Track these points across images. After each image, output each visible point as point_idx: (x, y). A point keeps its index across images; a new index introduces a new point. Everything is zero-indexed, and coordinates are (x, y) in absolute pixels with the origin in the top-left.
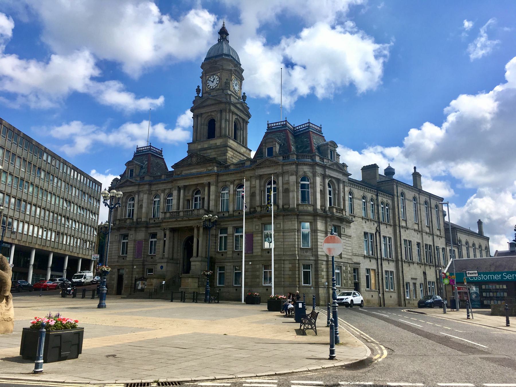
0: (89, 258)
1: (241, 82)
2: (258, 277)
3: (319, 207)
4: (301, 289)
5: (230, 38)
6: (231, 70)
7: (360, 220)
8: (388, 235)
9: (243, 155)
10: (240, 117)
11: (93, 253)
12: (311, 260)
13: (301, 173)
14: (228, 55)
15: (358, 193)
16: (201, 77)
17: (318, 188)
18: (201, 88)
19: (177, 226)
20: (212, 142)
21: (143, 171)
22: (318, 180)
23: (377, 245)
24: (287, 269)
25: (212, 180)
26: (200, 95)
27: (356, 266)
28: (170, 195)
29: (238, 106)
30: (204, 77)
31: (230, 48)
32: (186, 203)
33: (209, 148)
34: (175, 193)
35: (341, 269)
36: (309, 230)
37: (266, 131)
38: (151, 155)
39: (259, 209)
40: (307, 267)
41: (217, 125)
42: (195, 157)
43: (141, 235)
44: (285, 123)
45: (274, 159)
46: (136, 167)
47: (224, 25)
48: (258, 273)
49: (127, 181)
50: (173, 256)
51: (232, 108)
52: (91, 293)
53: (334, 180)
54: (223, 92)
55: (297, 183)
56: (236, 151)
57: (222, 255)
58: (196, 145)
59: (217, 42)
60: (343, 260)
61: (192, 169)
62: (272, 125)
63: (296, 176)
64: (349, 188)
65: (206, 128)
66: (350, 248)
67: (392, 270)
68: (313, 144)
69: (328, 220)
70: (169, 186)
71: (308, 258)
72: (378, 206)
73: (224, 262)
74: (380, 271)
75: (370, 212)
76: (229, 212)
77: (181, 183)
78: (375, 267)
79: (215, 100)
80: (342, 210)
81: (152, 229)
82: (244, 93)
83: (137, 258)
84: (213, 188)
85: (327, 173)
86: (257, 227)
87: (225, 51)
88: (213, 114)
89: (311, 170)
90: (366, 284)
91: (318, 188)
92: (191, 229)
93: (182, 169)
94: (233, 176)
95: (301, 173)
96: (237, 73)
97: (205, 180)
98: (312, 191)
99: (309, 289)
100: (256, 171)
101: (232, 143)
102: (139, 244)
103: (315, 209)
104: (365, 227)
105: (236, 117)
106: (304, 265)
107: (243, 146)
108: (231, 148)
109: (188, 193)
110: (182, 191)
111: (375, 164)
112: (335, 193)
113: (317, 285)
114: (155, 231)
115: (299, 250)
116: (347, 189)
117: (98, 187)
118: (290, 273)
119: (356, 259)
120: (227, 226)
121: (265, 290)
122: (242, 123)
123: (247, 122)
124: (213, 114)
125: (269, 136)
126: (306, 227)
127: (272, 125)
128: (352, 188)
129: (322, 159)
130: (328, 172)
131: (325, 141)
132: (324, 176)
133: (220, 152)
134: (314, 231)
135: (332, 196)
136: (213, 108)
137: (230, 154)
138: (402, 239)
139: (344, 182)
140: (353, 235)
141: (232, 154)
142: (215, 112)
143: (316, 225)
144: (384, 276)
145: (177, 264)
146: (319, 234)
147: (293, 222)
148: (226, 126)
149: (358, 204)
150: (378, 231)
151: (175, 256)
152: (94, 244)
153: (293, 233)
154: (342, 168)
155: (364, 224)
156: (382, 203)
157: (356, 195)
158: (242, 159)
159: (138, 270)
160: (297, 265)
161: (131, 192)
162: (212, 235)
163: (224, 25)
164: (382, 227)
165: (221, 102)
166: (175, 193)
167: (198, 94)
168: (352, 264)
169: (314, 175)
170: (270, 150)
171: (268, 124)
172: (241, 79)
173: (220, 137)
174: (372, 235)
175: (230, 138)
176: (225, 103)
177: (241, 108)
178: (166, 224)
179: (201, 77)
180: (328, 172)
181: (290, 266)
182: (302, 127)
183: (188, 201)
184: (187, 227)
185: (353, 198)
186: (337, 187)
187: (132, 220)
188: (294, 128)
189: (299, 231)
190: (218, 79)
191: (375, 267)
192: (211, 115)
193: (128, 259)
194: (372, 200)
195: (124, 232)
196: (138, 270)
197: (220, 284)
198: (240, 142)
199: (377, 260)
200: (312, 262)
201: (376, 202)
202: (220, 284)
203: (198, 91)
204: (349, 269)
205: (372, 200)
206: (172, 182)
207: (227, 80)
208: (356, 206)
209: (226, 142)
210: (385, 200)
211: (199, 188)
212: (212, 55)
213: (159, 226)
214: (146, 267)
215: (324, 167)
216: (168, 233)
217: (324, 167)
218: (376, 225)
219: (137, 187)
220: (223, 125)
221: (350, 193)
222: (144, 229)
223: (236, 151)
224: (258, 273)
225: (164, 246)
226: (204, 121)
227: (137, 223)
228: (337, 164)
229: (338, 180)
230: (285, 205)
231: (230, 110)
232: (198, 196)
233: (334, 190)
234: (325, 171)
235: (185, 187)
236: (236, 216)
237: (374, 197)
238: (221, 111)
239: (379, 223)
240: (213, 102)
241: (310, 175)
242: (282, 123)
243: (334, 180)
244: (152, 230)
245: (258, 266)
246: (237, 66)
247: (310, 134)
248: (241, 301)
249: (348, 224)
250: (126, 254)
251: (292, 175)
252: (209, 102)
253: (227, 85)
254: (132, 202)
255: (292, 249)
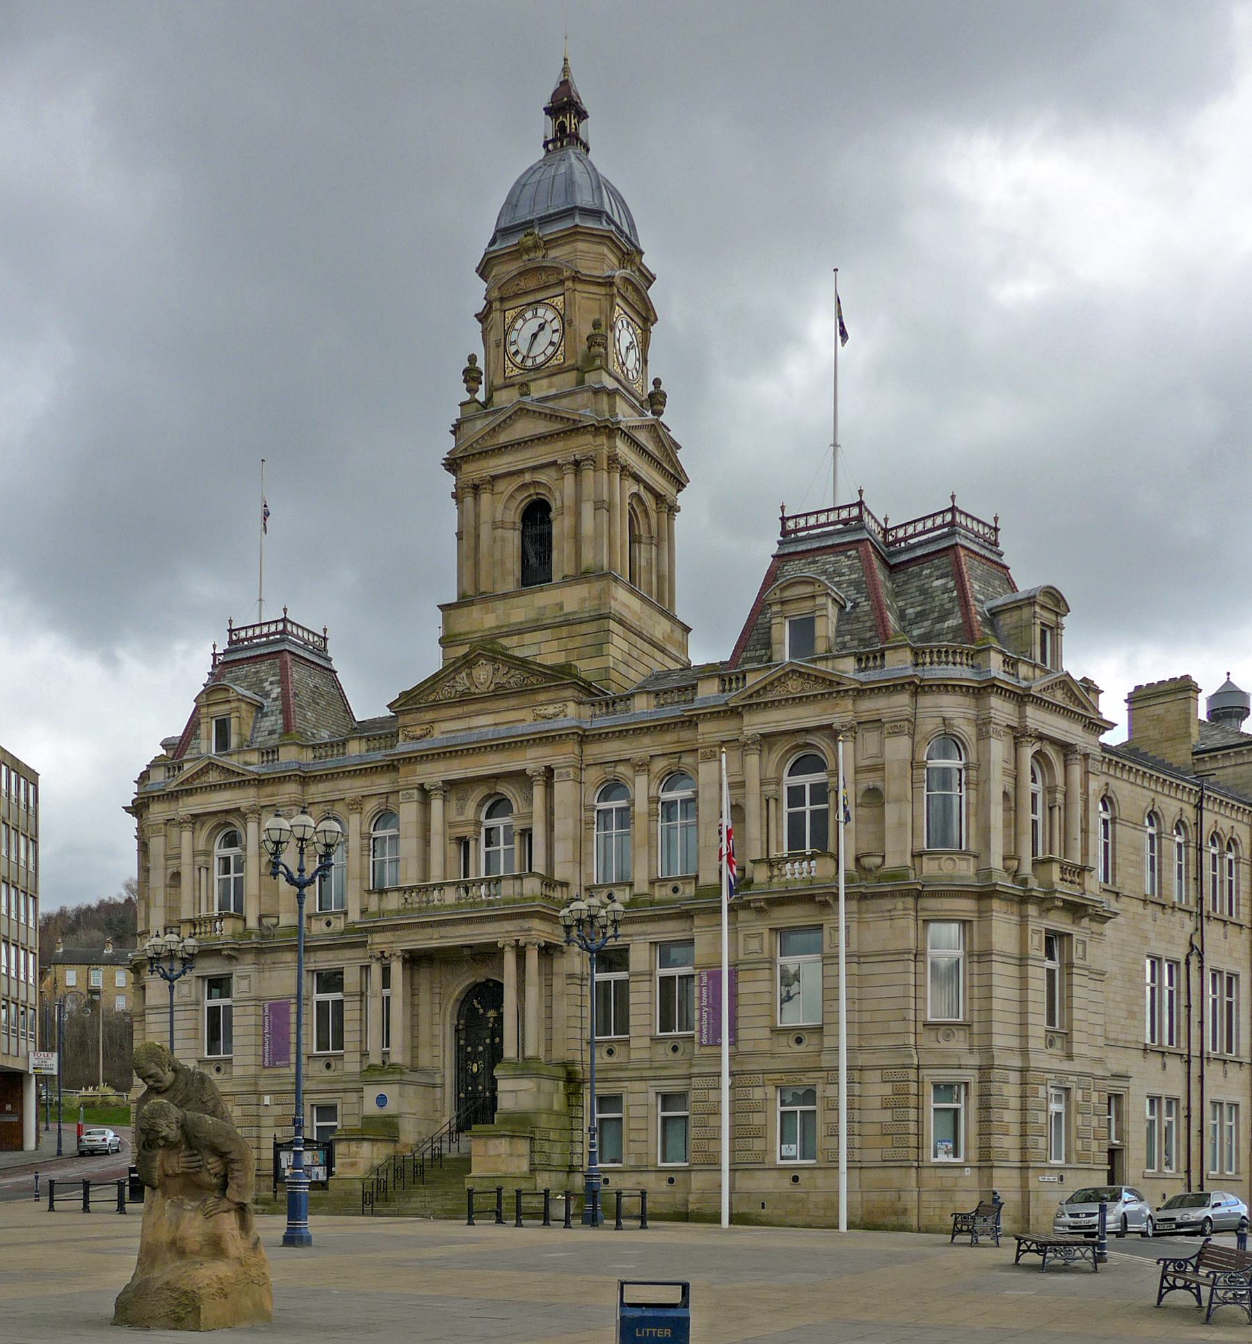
0: (18, 1065)
1: (646, 332)
2: (759, 1133)
3: (997, 862)
4: (926, 1173)
5: (590, 130)
6: (609, 282)
7: (1138, 907)
8: (1228, 967)
9: (663, 650)
10: (649, 488)
11: (31, 1046)
12: (967, 1067)
13: (929, 725)
14: (597, 214)
15: (1133, 795)
16: (482, 317)
17: (998, 783)
18: (481, 364)
19: (435, 944)
20: (543, 599)
21: (267, 723)
22: (999, 749)
23: (1189, 1007)
24: (877, 1103)
25: (561, 756)
26: (481, 396)
27: (1115, 1086)
28: (386, 816)
29: (642, 437)
30: (496, 315)
31: (599, 184)
32: (453, 849)
33: (537, 626)
34: (409, 812)
35: (1068, 1099)
36: (960, 953)
37: (775, 549)
38: (289, 657)
39: (760, 875)
40: (944, 1089)
41: (560, 527)
42: (475, 664)
43: (280, 979)
44: (855, 512)
45: (821, 666)
46: (238, 710)
47: (565, 70)
48: (757, 1119)
49: (211, 766)
50: (414, 1057)
51: (622, 449)
52: (113, 1193)
53: (1050, 751)
54: (581, 382)
55: (915, 764)
56: (640, 635)
57: (610, 1052)
58: (475, 611)
59: (543, 152)
60: (1076, 1066)
61: (477, 714)
62: (802, 522)
63: (912, 736)
64: (1104, 779)
65: (513, 539)
66: (1099, 1020)
67: (1234, 1099)
68: (972, 602)
69: (1032, 910)
70: (382, 783)
71: (954, 1061)
72: (1200, 849)
73: (619, 1080)
74: (1195, 1105)
75: (1171, 876)
76: (631, 885)
77: (433, 774)
78: (1178, 1091)
79: (551, 417)
80: (1083, 870)
81: (320, 956)
82: (657, 382)
83: (273, 1065)
84: (564, 791)
85: (1031, 724)
86: (754, 944)
87: (584, 199)
88: (542, 477)
89: (971, 713)
90: (1144, 1155)
91: (998, 783)
92: (489, 954)
93: (430, 716)
94: (647, 740)
95: (929, 725)
96: (631, 295)
97: (531, 760)
98: (973, 799)
99: (956, 1172)
100: (746, 719)
101: (623, 600)
102: (277, 1015)
103: (985, 872)
104: (1152, 935)
105: (634, 488)
106: (936, 1086)
107: (663, 613)
108: (621, 622)
109: (461, 810)
110: (437, 804)
111: (1186, 678)
112: (1057, 803)
113: (986, 1161)
114: (336, 965)
115: (920, 1026)
116: (1095, 785)
117: (27, 790)
118: (887, 1116)
119: (1117, 1061)
120: (627, 940)
121: (786, 1183)
122: (653, 515)
123: (673, 509)
124: (542, 477)
125: (793, 569)
126: (945, 942)
127: (802, 522)
128: (1112, 781)
129: (1011, 663)
130: (1036, 718)
131: (1014, 588)
132: (1019, 735)
133: (578, 642)
134: (981, 956)
135: (1039, 817)
136: (543, 454)
137: (618, 645)
138: (1207, 966)
139: (1086, 756)
140: (1111, 968)
141: (625, 646)
142: (552, 472)
143: (987, 935)
144: (1209, 1121)
145: (434, 1086)
146: (997, 968)
147: (902, 922)
148: (589, 524)
149: (1134, 839)
150: (1197, 950)
151: (424, 1059)
152: (31, 1012)
153: (899, 967)
154: (1079, 698)
155: (1148, 925)
156: (1216, 837)
157: (1124, 811)
158: (657, 668)
159: (278, 1110)
160: (913, 1088)
161: (227, 812)
162: (571, 976)
163: (565, 70)
164: (1213, 931)
165: (574, 429)
166: (409, 812)
167: (472, 391)
168: (1104, 1078)
169: (983, 733)
170: (803, 630)
171: (784, 520)
172: (646, 317)
173: (582, 576)
174: (1173, 964)
175: (616, 579)
176: (597, 430)
177: (651, 447)
178: (389, 936)
179: (482, 317)
180: (1036, 718)
181: (887, 1089)
182: (920, 527)
183: (463, 842)
184: (470, 946)
185: (1114, 820)
186: (1060, 780)
187: (240, 924)
188: (886, 531)
189: (919, 955)
190: (556, 324)
191: (1178, 1091)
192: (536, 484)
193: (237, 1071)
194: (1180, 825)
195: (213, 968)
196: (278, 1110)
197: (664, 1161)
198: (650, 593)
199: (1189, 1062)
200: (972, 1077)
201: (1192, 836)
202: (664, 1161)
203: (471, 376)
204: (1095, 1097)
205: (1180, 825)
206: (392, 767)
207: (596, 325)
208: (1123, 854)
209: (603, 597)
210: (1225, 825)
211: (506, 790)
212: (524, 215)
213: (363, 944)
214: (308, 1100)
215: (1021, 698)
216: (397, 968)
217: (1021, 698)
218: (1190, 925)
219: (252, 792)
220: (588, 525)
221: (1107, 801)
222: (290, 957)
223: (640, 635)
224: (757, 1119)
225: (408, 1028)
226: (503, 508)
227: (265, 932)
228: (1066, 683)
229: (1066, 749)
230: (869, 855)
231: (613, 459)
232: (499, 822)
233: (1050, 790)
234: (1022, 716)
235: (452, 787)
236: (660, 903)
237: (1190, 814)
238: (577, 463)
239: (1201, 917)
240: (542, 427)
241: (966, 730)
242: (844, 514)
243: (1050, 751)
244: (325, 961)
245: (758, 1094)
246: (632, 262)
247: (957, 558)
248: (719, 1221)
249: (1095, 927)
250: (228, 1050)
251: (896, 733)
252: (525, 428)
253: (596, 348)
254: (232, 852)
255: (894, 1027)
